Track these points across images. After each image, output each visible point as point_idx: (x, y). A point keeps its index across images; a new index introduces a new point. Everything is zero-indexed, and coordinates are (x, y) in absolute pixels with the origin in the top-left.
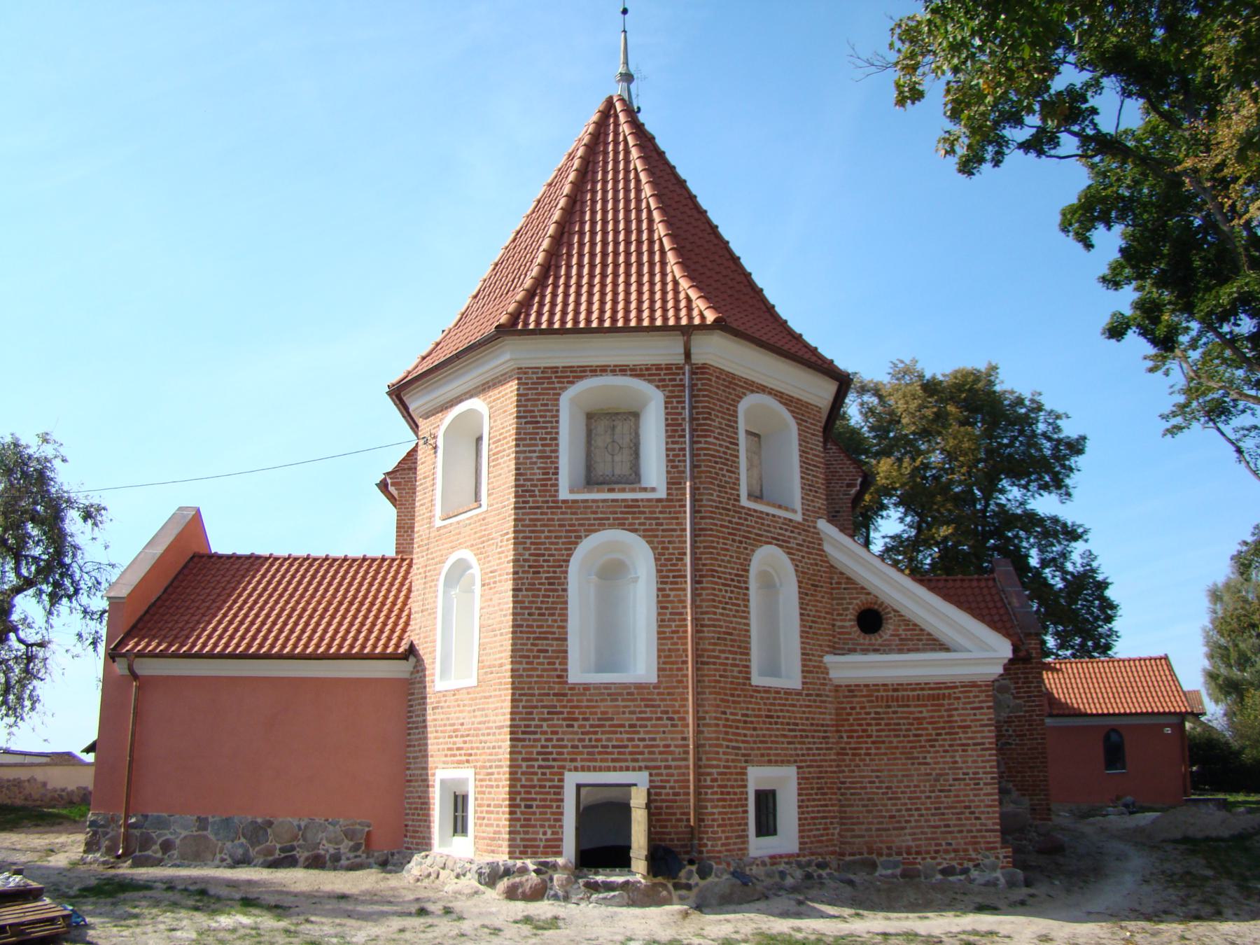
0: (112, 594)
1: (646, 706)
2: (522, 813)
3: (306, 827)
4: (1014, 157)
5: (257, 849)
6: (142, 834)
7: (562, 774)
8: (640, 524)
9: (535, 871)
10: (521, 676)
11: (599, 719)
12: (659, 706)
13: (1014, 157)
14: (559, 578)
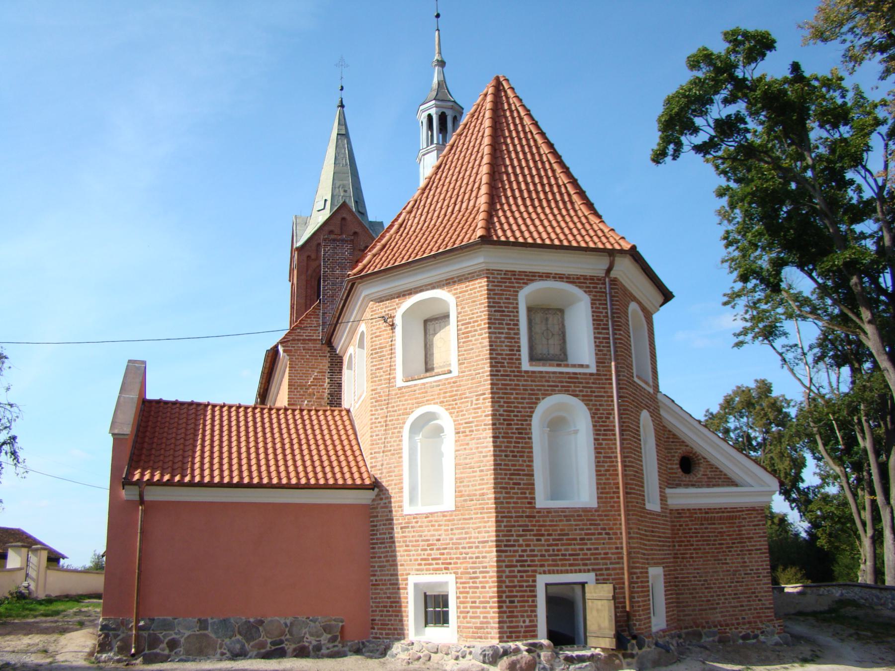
0: (116, 431)
1: (591, 524)
2: (508, 607)
3: (291, 623)
4: (688, 156)
5: (252, 643)
6: (149, 635)
7: (535, 576)
8: (580, 391)
9: (527, 651)
10: (502, 503)
11: (559, 535)
12: (599, 525)
13: (688, 156)
14: (526, 429)
